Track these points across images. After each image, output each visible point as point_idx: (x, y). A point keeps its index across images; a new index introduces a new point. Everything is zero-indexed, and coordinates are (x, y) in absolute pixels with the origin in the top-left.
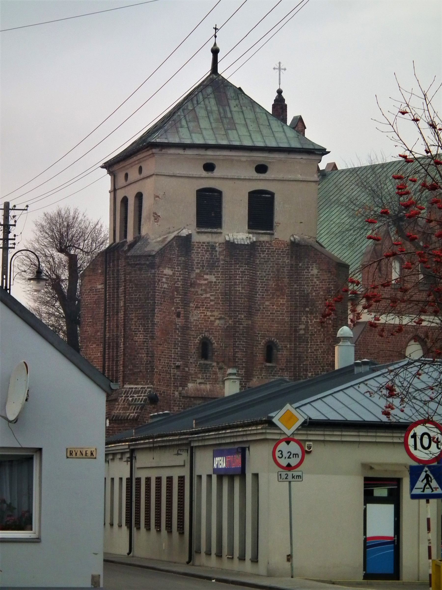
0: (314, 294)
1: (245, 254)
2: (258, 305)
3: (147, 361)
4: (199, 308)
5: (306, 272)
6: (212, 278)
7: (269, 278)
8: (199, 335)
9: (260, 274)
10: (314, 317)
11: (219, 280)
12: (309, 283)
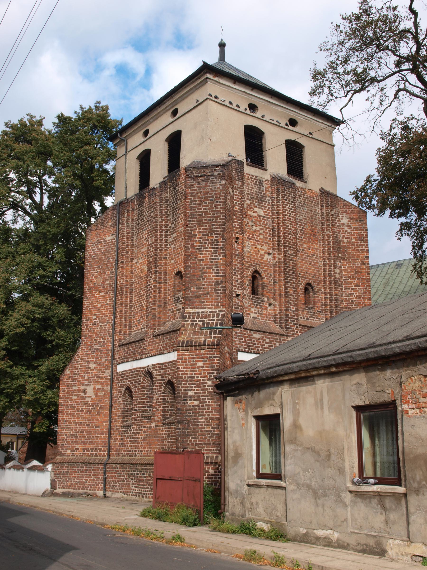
1: (291, 192)
3: (217, 282)
4: (251, 239)
6: (261, 212)
10: (347, 263)
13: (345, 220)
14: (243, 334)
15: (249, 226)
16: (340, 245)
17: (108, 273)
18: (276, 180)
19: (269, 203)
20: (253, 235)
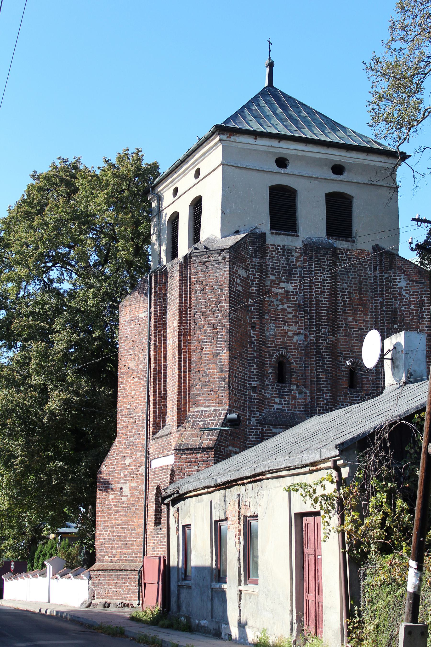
0: (403, 309)
1: (327, 260)
2: (341, 321)
4: (275, 320)
5: (393, 285)
6: (289, 287)
7: (352, 291)
8: (275, 353)
9: (341, 285)
11: (296, 289)
12: (397, 297)
13: (403, 284)
14: (259, 429)
15: (273, 305)
17: (142, 355)
18: (310, 247)
19: (300, 275)
20: (279, 315)
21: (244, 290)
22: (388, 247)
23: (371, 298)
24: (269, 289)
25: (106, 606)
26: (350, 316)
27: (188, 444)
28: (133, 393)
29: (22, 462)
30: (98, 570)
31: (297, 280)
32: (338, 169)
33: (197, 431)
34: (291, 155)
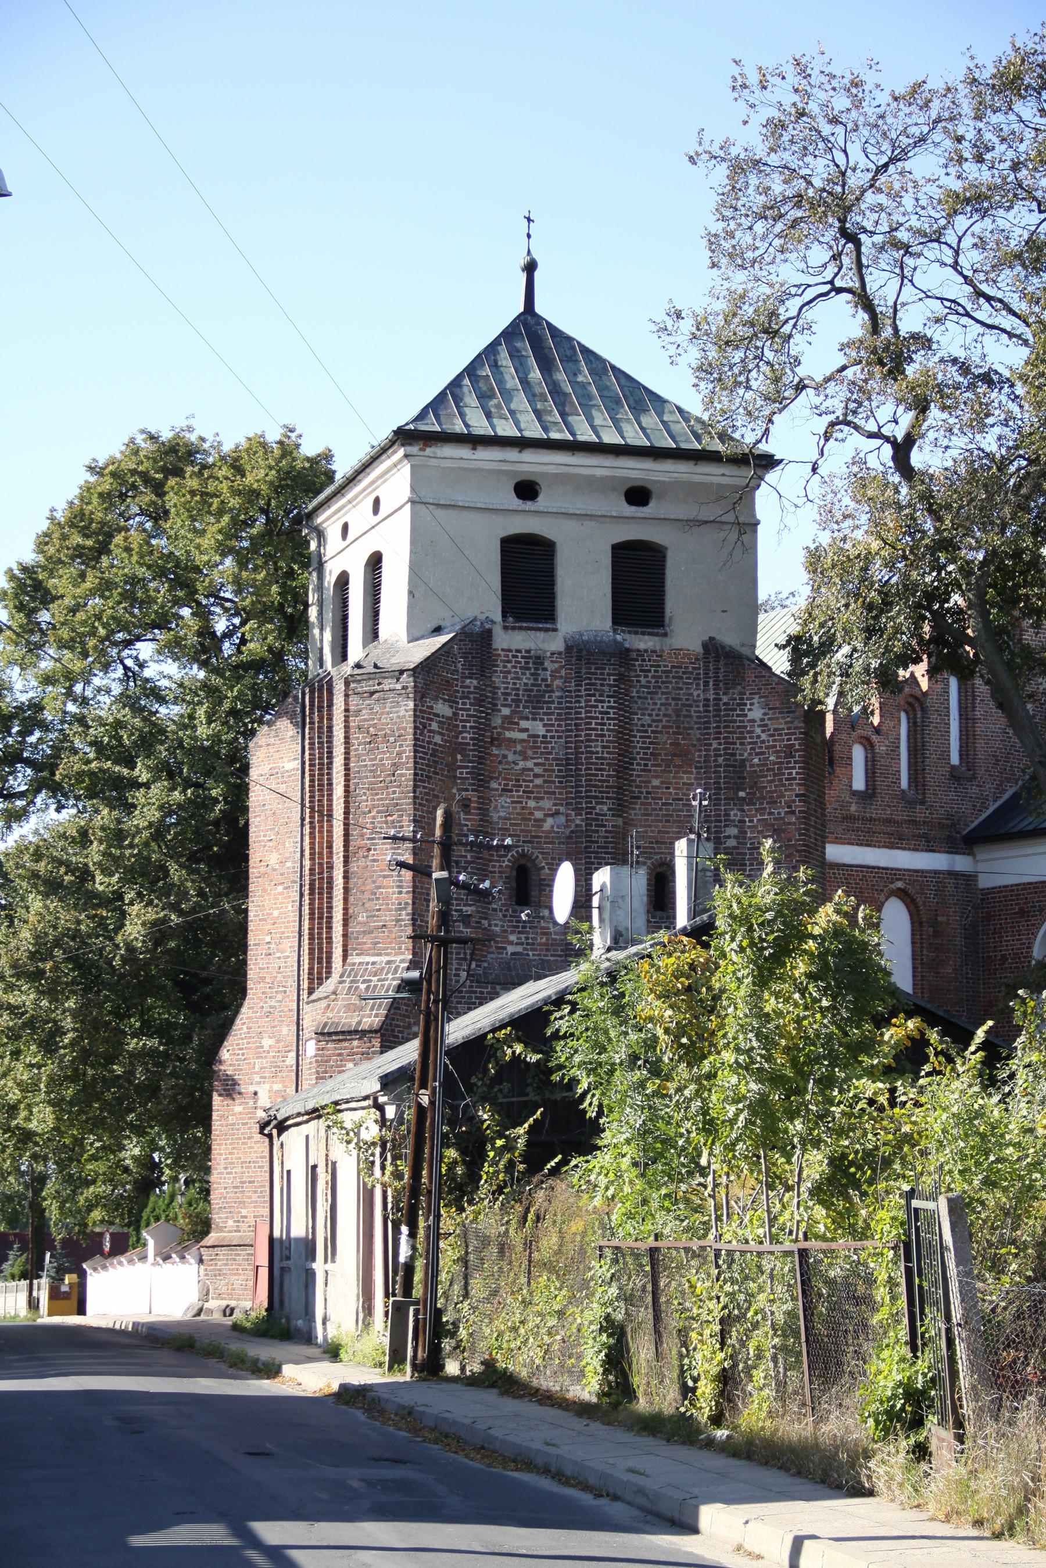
0: (756, 761)
4: (511, 791)
6: (539, 728)
13: (756, 713)
15: (507, 763)
16: (742, 772)
18: (579, 652)
20: (518, 780)
21: (446, 741)
22: (730, 639)
23: (699, 740)
24: (499, 734)
25: (228, 1312)
26: (657, 777)
27: (338, 1024)
28: (276, 914)
29: (73, 1043)
30: (214, 1247)
31: (552, 714)
32: (638, 495)
33: (354, 1000)
34: (543, 474)
